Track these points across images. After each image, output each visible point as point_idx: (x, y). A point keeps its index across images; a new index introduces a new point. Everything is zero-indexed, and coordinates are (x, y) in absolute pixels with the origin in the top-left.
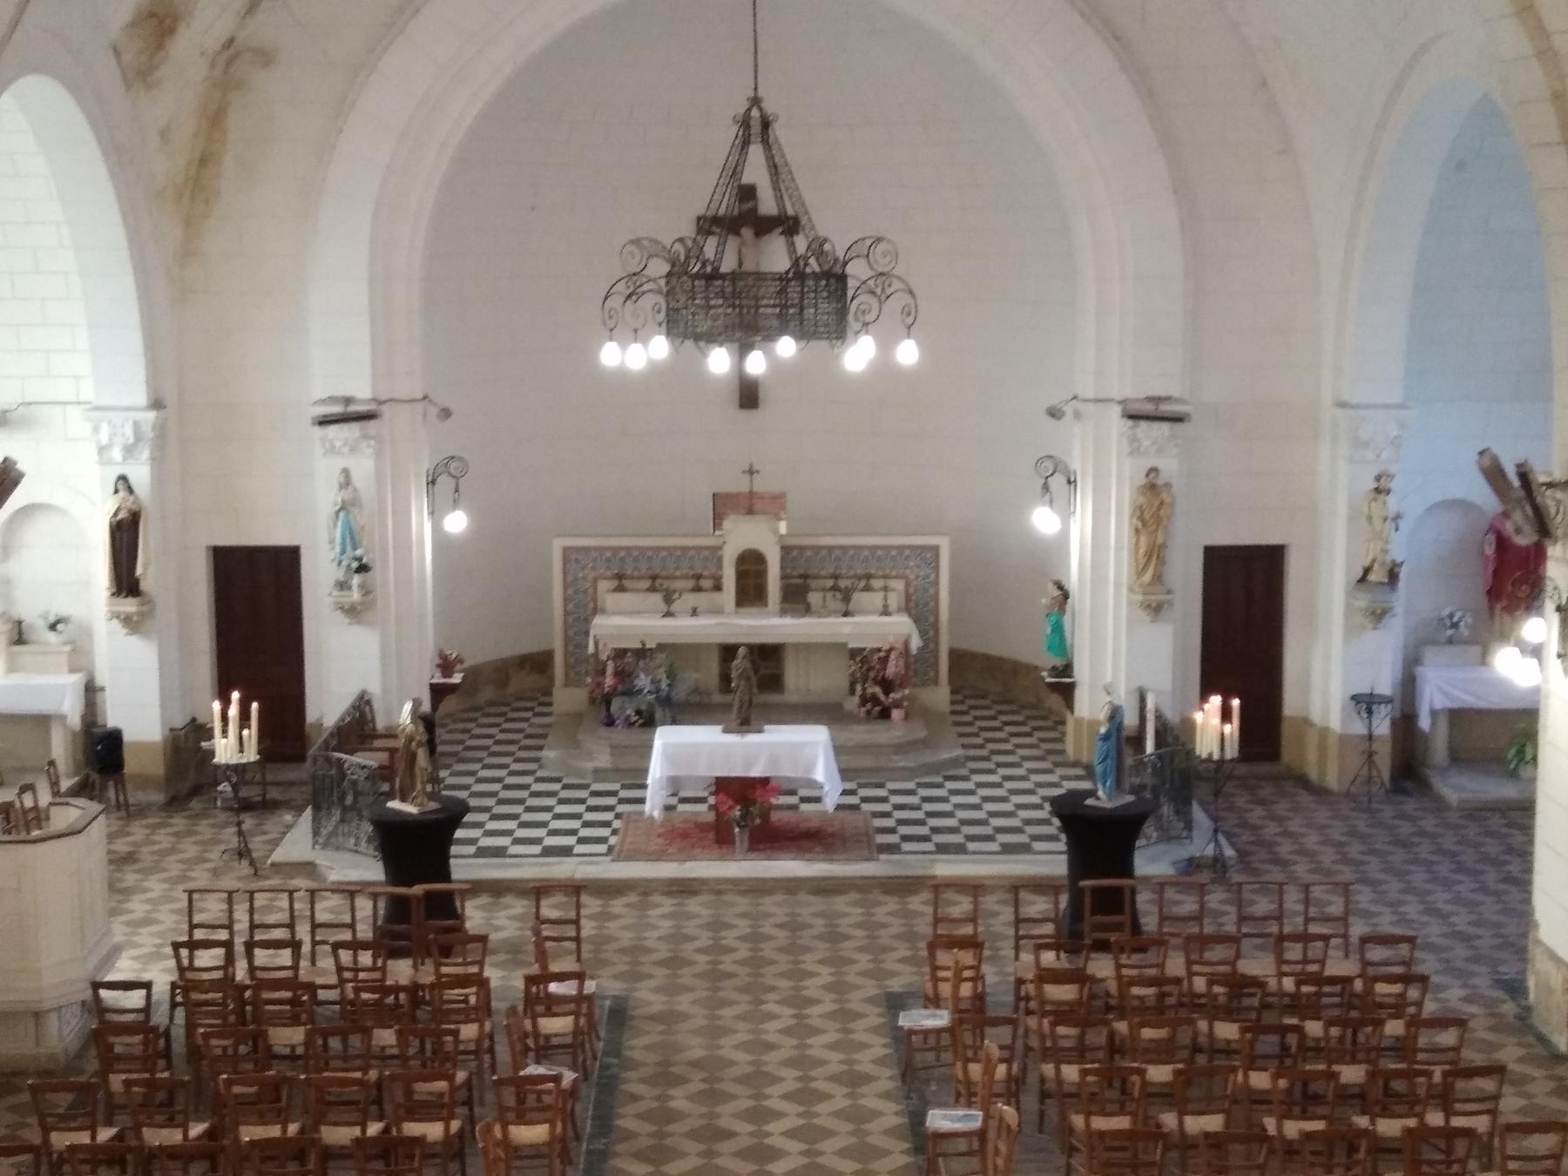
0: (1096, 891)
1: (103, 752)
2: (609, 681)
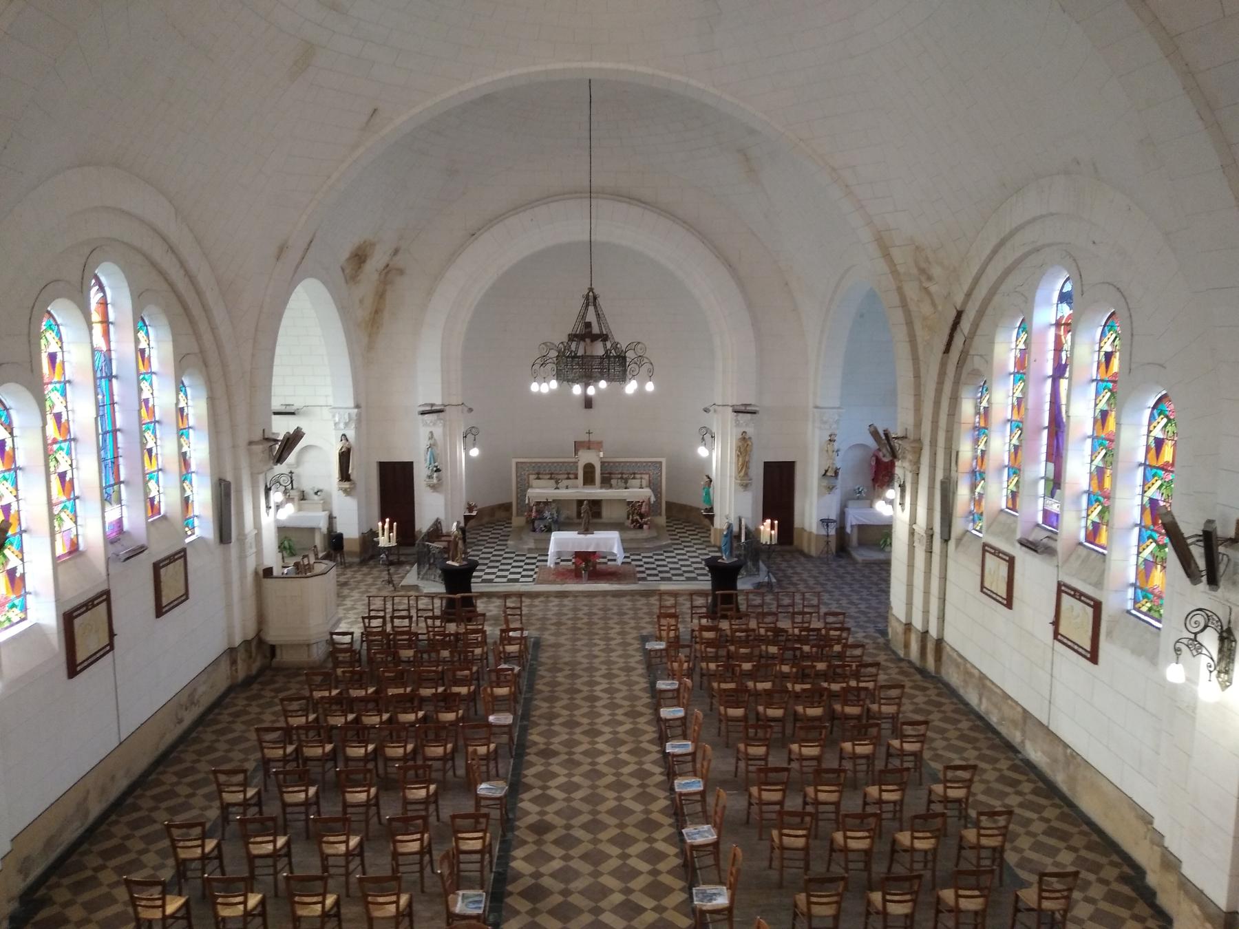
1: (335, 542)
2: (534, 514)
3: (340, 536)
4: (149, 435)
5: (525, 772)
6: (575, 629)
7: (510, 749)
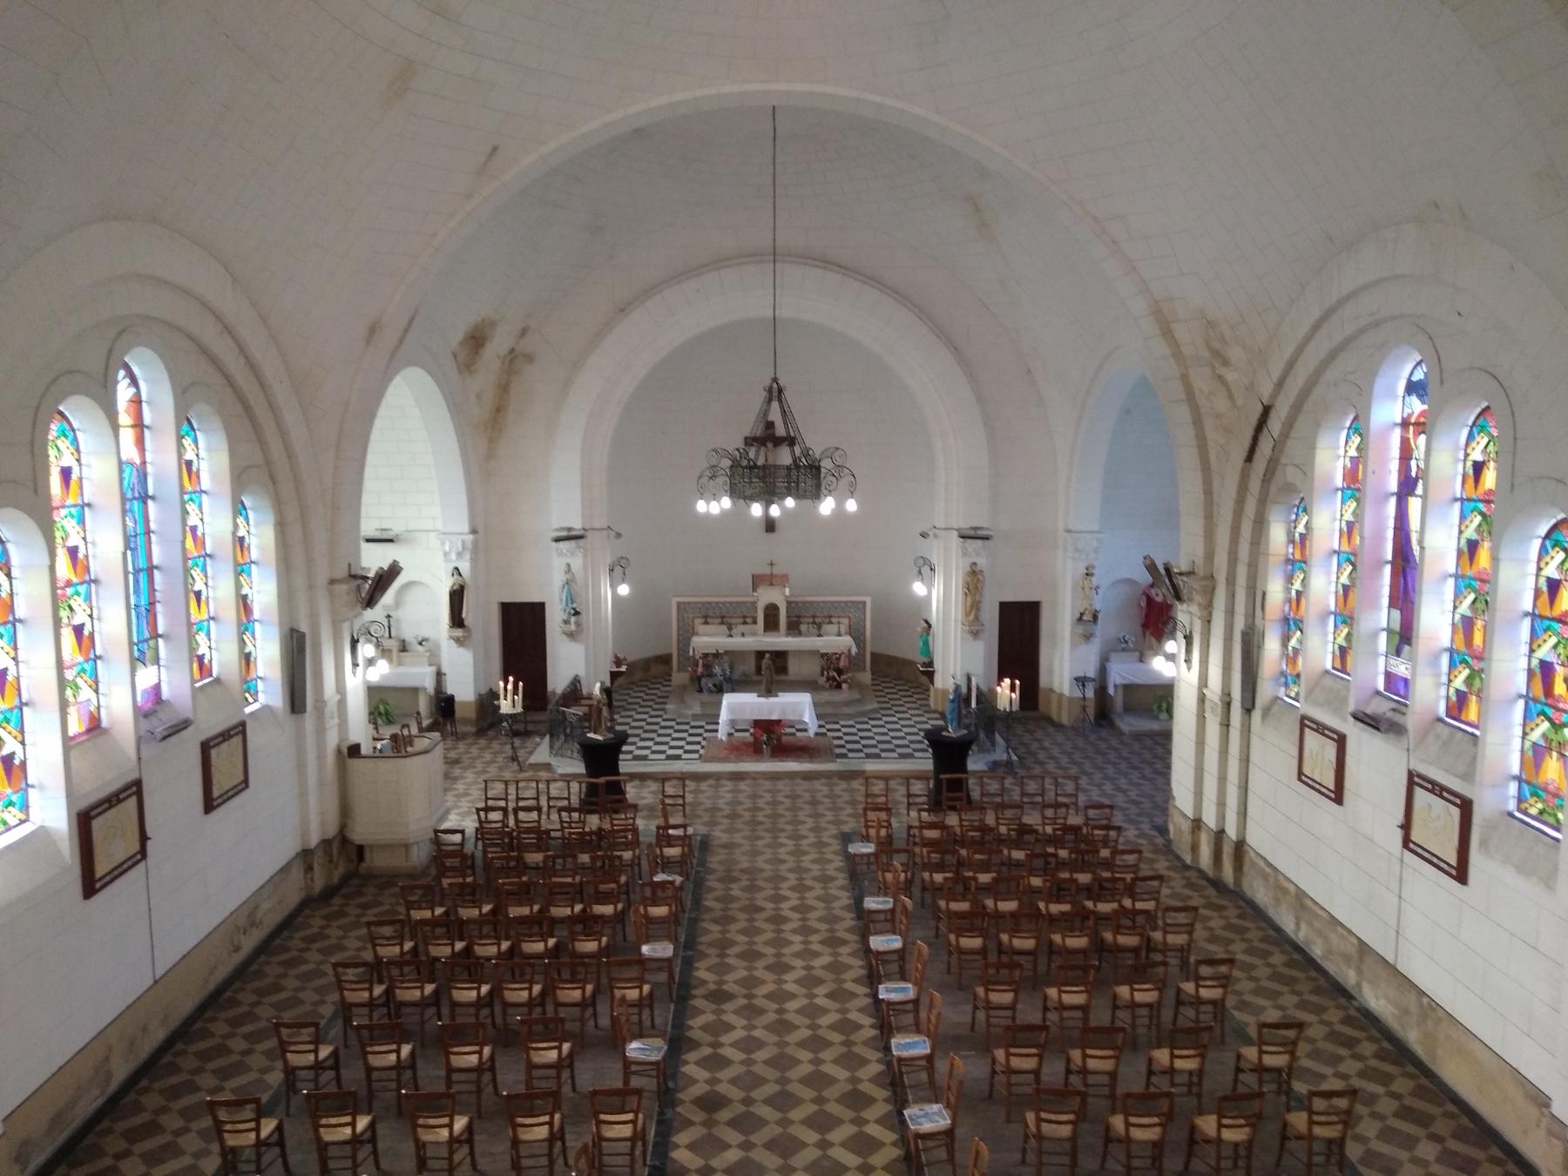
0: (948, 780)
1: (444, 706)
2: (700, 670)
3: (451, 698)
4: (197, 573)
7: (670, 989)
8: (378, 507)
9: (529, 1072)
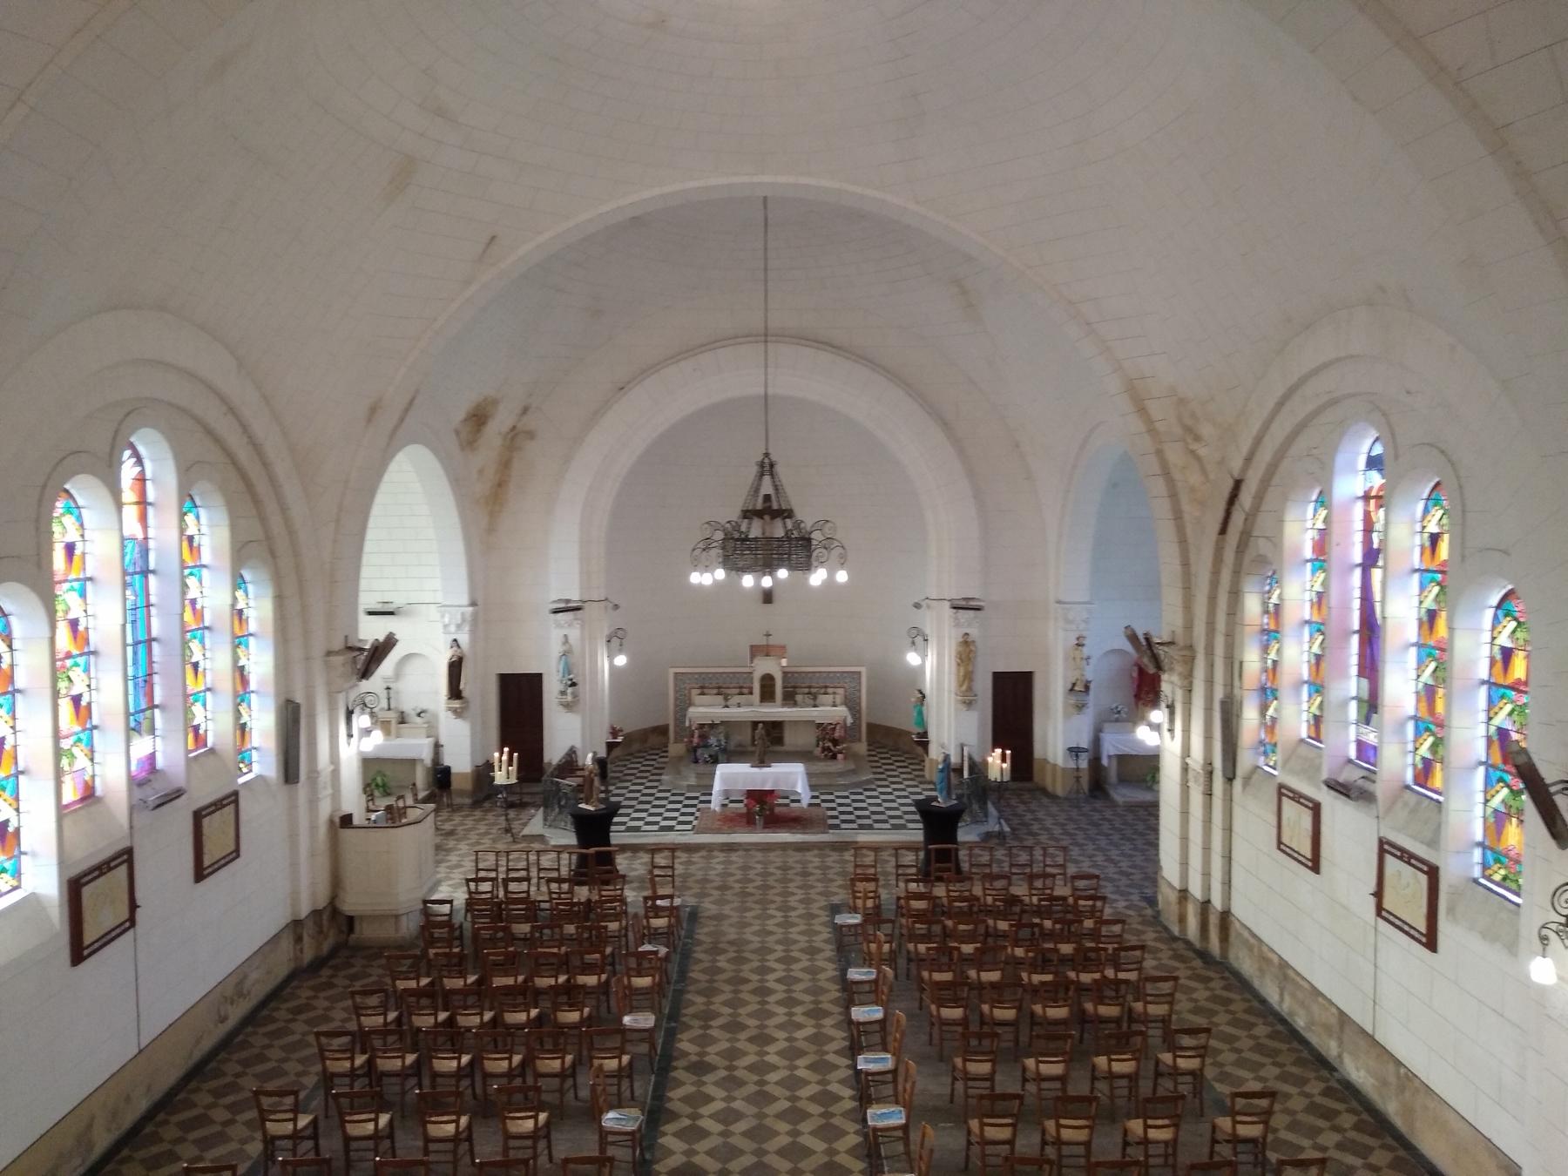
0: (937, 850)
1: (441, 777)
2: (696, 740)
3: (447, 770)
4: (195, 645)
5: (670, 1094)
6: (744, 894)
8: (378, 579)
9: (506, 1143)
